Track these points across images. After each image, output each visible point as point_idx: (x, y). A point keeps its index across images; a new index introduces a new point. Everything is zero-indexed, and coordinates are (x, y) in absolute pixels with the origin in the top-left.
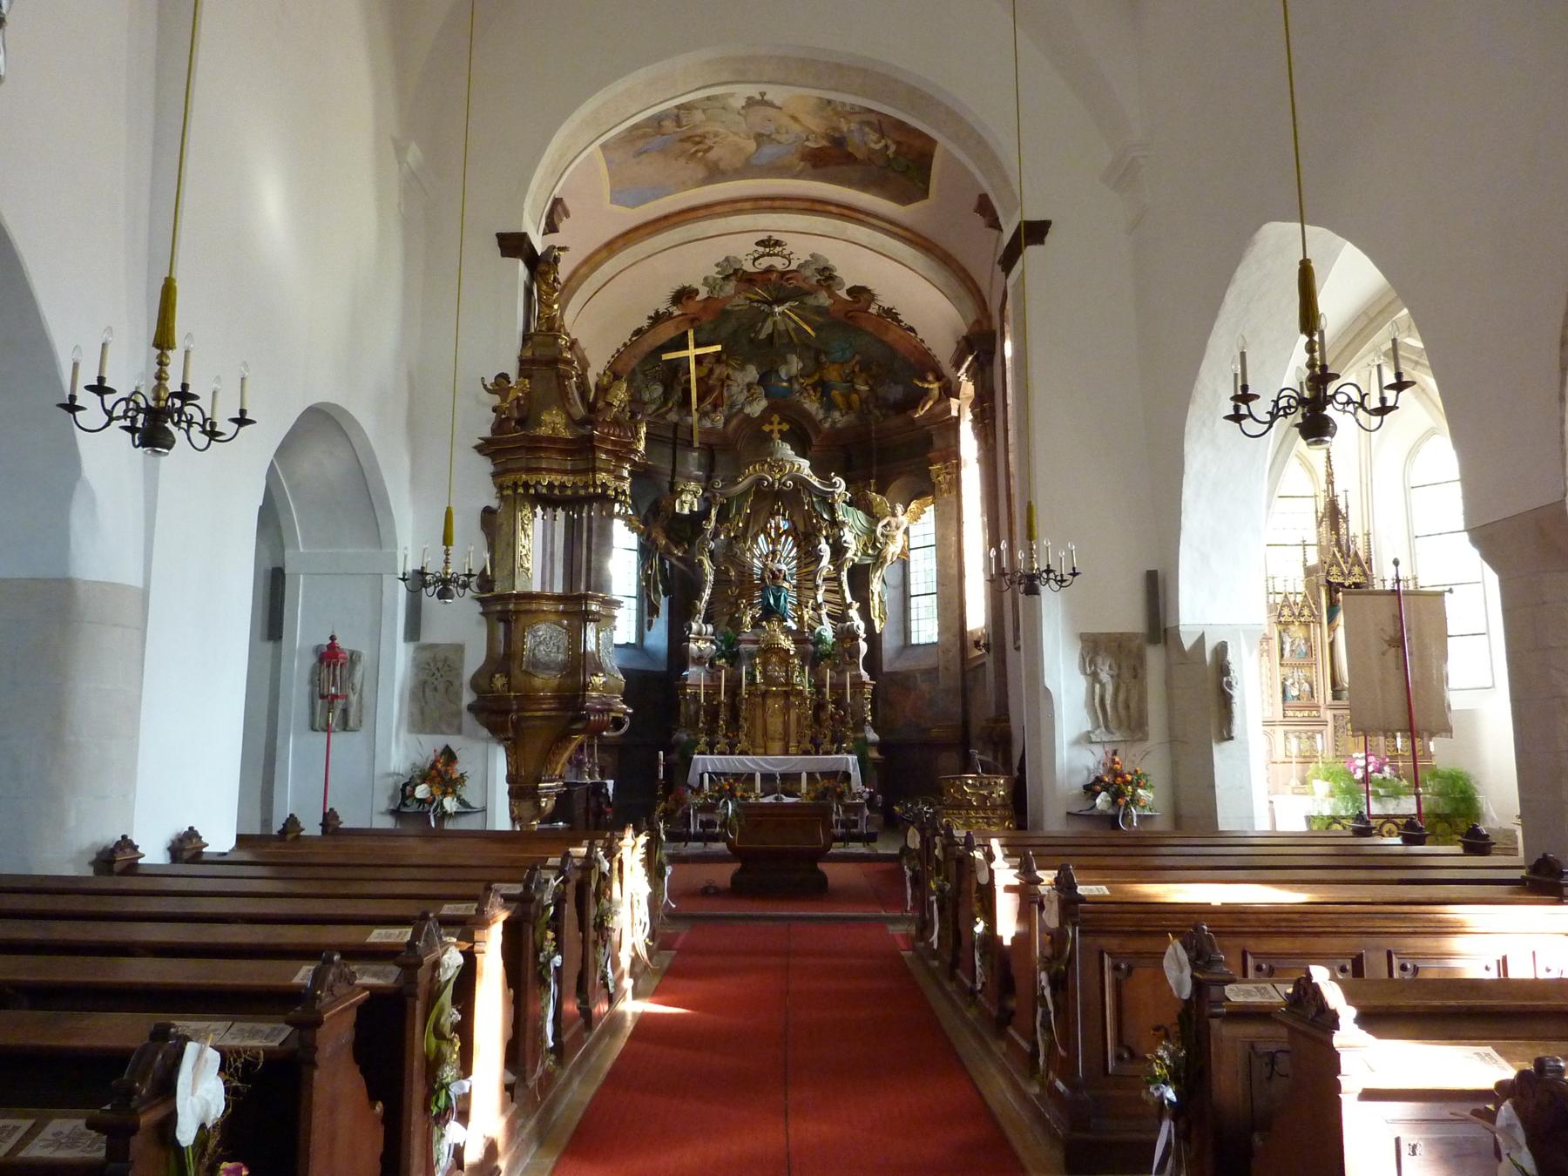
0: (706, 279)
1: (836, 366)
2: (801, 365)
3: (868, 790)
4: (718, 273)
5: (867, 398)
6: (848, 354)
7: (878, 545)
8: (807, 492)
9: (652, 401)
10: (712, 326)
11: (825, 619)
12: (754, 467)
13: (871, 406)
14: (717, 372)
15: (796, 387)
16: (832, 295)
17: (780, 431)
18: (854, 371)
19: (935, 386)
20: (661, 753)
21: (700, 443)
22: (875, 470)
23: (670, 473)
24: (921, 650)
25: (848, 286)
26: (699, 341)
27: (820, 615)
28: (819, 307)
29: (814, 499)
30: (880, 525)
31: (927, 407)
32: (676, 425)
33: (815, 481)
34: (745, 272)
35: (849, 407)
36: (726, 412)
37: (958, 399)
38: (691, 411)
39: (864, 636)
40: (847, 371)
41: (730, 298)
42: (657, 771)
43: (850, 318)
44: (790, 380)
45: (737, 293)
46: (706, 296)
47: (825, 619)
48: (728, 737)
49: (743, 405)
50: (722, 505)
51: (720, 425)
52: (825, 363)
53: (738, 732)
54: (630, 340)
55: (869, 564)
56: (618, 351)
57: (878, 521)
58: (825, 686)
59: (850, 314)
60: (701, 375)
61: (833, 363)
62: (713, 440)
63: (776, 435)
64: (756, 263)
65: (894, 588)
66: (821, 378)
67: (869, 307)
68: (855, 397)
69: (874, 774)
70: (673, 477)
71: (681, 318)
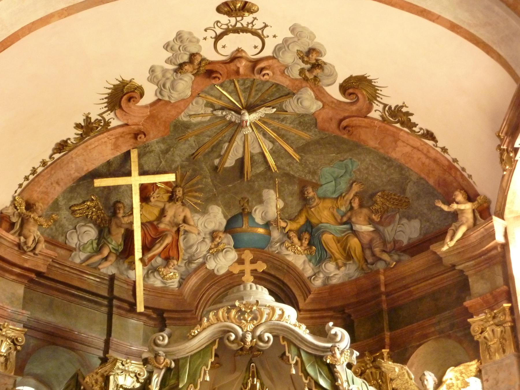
0: (152, 70)
1: (328, 203)
2: (281, 204)
4: (169, 61)
5: (371, 241)
6: (343, 185)
8: (294, 350)
9: (82, 248)
10: (163, 147)
12: (216, 315)
13: (377, 250)
14: (170, 214)
15: (276, 234)
17: (254, 272)
18: (352, 208)
19: (468, 207)
21: (146, 307)
22: (387, 334)
23: (102, 345)
25: (340, 80)
26: (146, 168)
28: (303, 116)
31: (459, 235)
32: (112, 278)
33: (303, 331)
34: (203, 59)
35: (349, 257)
36: (183, 269)
37: (503, 218)
38: (134, 262)
40: (343, 209)
41: (186, 102)
43: (345, 128)
44: (267, 225)
45: (195, 95)
46: (154, 99)
49: (205, 257)
50: (169, 370)
51: (174, 284)
52: (313, 197)
54: (51, 157)
56: (34, 171)
59: (344, 123)
60: (151, 217)
61: (323, 198)
62: (164, 304)
63: (248, 278)
66: (308, 221)
67: (369, 110)
68: (354, 242)
70: (106, 350)
71: (120, 130)
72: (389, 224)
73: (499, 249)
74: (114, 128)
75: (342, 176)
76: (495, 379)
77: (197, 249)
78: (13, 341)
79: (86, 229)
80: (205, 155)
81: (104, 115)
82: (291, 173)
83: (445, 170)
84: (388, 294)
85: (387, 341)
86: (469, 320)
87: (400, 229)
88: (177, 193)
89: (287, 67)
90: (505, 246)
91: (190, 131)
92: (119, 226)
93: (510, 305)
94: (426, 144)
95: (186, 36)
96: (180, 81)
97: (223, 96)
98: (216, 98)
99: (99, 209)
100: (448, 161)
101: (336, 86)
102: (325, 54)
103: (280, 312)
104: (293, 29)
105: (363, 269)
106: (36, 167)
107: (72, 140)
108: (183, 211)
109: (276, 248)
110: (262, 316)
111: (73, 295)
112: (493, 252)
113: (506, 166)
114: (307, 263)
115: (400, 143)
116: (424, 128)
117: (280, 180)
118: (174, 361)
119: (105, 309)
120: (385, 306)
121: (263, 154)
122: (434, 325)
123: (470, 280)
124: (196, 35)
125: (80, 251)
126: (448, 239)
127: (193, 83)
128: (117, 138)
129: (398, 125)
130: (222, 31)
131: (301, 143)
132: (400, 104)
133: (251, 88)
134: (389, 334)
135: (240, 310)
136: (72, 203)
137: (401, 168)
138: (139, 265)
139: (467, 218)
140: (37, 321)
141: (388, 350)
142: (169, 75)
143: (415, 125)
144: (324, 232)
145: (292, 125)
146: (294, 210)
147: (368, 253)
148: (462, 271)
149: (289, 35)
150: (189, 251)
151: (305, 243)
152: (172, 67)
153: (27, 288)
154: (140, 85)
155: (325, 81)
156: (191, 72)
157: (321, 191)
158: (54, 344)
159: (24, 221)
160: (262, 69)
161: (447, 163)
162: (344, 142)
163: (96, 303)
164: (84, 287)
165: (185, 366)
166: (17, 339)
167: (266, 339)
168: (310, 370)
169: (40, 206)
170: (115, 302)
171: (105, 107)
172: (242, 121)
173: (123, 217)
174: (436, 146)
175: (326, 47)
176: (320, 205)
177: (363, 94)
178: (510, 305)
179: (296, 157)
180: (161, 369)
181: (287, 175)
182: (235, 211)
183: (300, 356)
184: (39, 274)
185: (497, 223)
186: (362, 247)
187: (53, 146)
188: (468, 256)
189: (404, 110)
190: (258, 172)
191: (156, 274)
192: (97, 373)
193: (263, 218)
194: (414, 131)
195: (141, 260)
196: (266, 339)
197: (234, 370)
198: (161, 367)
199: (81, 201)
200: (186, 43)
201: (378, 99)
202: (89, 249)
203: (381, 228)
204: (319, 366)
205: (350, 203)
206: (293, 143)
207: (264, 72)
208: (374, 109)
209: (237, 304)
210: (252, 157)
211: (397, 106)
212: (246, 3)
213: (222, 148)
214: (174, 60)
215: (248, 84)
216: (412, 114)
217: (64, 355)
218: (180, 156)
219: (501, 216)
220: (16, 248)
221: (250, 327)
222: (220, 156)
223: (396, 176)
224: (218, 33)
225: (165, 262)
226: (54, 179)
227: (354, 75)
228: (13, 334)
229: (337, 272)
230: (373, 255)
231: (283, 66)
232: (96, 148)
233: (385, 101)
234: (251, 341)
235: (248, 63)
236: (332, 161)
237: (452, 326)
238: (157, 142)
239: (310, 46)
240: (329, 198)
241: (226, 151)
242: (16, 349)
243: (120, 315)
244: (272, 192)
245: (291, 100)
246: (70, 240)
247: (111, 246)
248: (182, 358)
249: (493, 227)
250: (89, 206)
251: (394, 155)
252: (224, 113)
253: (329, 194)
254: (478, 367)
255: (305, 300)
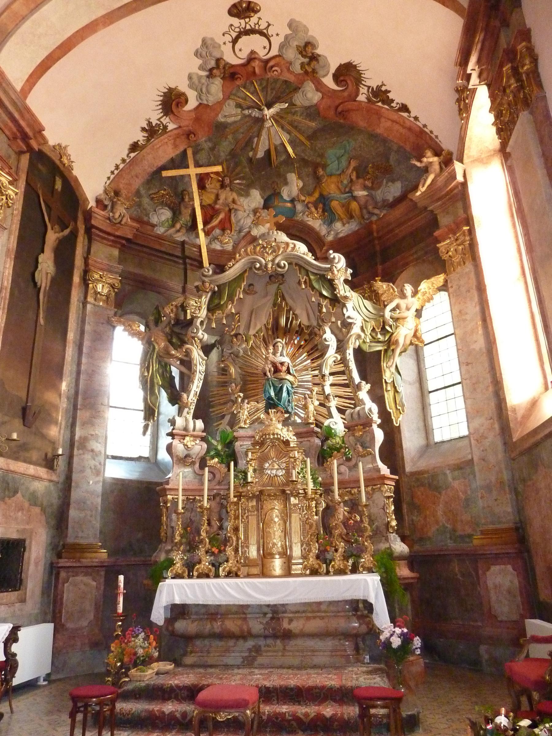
0: (190, 77)
1: (334, 179)
2: (301, 184)
3: (398, 631)
4: (201, 68)
5: (367, 201)
6: (344, 163)
7: (388, 328)
8: (303, 272)
9: (162, 224)
10: (210, 144)
11: (334, 411)
13: (370, 208)
14: (222, 197)
15: (299, 207)
16: (319, 86)
18: (351, 181)
19: (436, 159)
20: (121, 578)
22: (380, 268)
24: (446, 446)
25: (333, 70)
27: (329, 409)
28: (309, 107)
29: (312, 277)
30: (389, 308)
31: (429, 182)
33: (310, 257)
36: (235, 237)
39: (379, 421)
41: (220, 104)
42: (116, 603)
44: (292, 201)
45: (227, 97)
47: (334, 411)
48: (213, 554)
50: (214, 293)
52: (323, 175)
53: (225, 546)
54: (128, 156)
55: (380, 351)
56: (117, 167)
57: (385, 306)
58: (333, 484)
59: (340, 109)
61: (331, 175)
64: (237, 47)
65: (410, 384)
66: (321, 196)
68: (354, 205)
69: (407, 600)
72: (379, 188)
73: (460, 188)
74: (171, 130)
75: (342, 156)
76: (457, 285)
77: (244, 222)
78: (111, 286)
79: (163, 211)
80: (241, 150)
81: (161, 120)
82: (306, 158)
83: (417, 136)
84: (379, 238)
85: (380, 271)
86: (438, 245)
87: (387, 190)
88: (226, 181)
89: (291, 63)
90: (464, 185)
91: (227, 130)
92: (186, 208)
93: (468, 228)
94: (403, 116)
95: (209, 42)
96: (212, 85)
97: (247, 97)
98: (242, 99)
99: (170, 196)
100: (420, 127)
101: (330, 76)
102: (318, 46)
103: (293, 246)
104: (290, 25)
105: (361, 223)
106: (118, 164)
107: (142, 142)
108: (231, 195)
109: (299, 217)
110: (279, 249)
111: (158, 257)
112: (455, 191)
113: (463, 114)
114: (322, 226)
115: (383, 120)
116: (400, 103)
117: (298, 165)
118: (217, 286)
119: (182, 266)
120: (378, 248)
121: (283, 145)
122: (412, 255)
123: (438, 217)
124: (217, 41)
125: (160, 226)
126: (420, 187)
127: (223, 86)
128: (175, 139)
129: (380, 104)
130: (237, 34)
131: (310, 132)
132: (380, 84)
133: (266, 87)
134: (381, 266)
135: (263, 247)
136: (151, 192)
137: (385, 141)
138: (202, 235)
139: (435, 169)
140: (130, 273)
141: (380, 278)
142: (203, 81)
143: (392, 101)
144: (332, 200)
145: (302, 117)
146: (311, 187)
147: (365, 211)
148: (432, 211)
149: (289, 32)
150: (239, 224)
151: (320, 211)
152: (204, 73)
153: (121, 251)
154: (183, 91)
155: (321, 72)
156: (219, 76)
157: (328, 170)
158: (144, 289)
159: (113, 205)
160: (272, 67)
161: (418, 129)
162: (341, 126)
163: (175, 262)
164: (163, 249)
165: (225, 289)
166: (114, 284)
167: (283, 265)
168: (316, 285)
169: (124, 192)
170: (188, 261)
171: (161, 113)
172: (263, 116)
173: (189, 202)
174: (410, 117)
175: (317, 38)
176: (329, 180)
177: (351, 80)
178: (468, 228)
179: (307, 143)
180: (208, 292)
181: (303, 160)
182: (268, 193)
183: (308, 275)
184: (128, 240)
185: (458, 167)
186: (360, 208)
187: (128, 147)
188: (435, 198)
189: (383, 88)
190: (282, 160)
191: (216, 241)
192: (172, 305)
193: (289, 196)
194: (392, 107)
195: (203, 230)
196: (283, 265)
197: (266, 295)
198: (208, 291)
199: (157, 190)
200: (211, 49)
201: (363, 82)
202: (166, 224)
203: (373, 192)
204: (322, 281)
205: (350, 176)
206: (304, 132)
207: (274, 69)
208: (361, 93)
209: (260, 242)
210: (276, 148)
211: (378, 86)
212: (250, 2)
213: (253, 143)
214: (204, 67)
215: (264, 84)
216: (389, 92)
217: (153, 296)
218: (224, 152)
219: (461, 160)
220: (108, 221)
221: (270, 258)
222: (252, 149)
223: (381, 149)
224: (234, 36)
225: (222, 232)
226: (133, 173)
227: (342, 63)
228: (111, 281)
229: (343, 228)
230: (369, 213)
231: (287, 62)
232: (161, 148)
233: (368, 84)
234: (272, 267)
235: (261, 63)
236: (334, 144)
237: (426, 253)
238: (206, 141)
239: (306, 40)
240: (335, 175)
241: (257, 144)
242: (114, 291)
243: (193, 270)
244: (293, 175)
245: (298, 94)
246: (153, 219)
247: (181, 222)
248: (223, 284)
249: (454, 169)
250: (163, 194)
251: (379, 131)
252: (250, 112)
253: (334, 172)
254: (445, 278)
255: (321, 251)
